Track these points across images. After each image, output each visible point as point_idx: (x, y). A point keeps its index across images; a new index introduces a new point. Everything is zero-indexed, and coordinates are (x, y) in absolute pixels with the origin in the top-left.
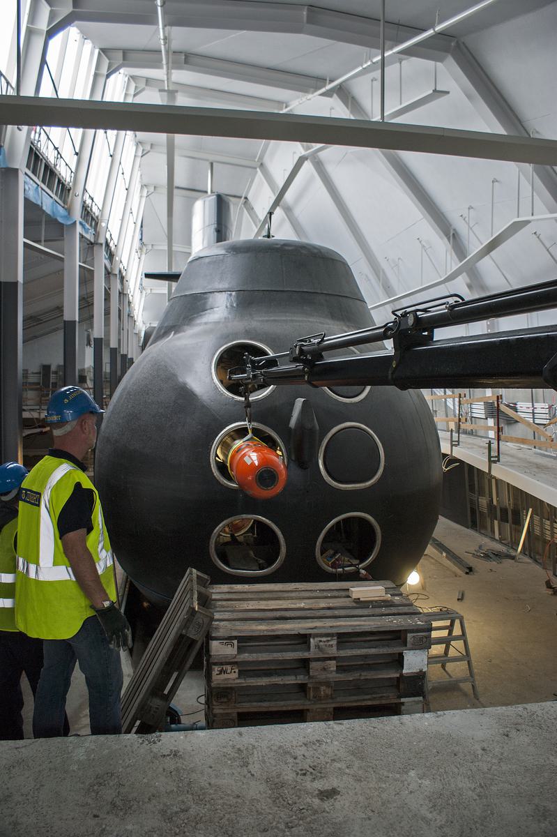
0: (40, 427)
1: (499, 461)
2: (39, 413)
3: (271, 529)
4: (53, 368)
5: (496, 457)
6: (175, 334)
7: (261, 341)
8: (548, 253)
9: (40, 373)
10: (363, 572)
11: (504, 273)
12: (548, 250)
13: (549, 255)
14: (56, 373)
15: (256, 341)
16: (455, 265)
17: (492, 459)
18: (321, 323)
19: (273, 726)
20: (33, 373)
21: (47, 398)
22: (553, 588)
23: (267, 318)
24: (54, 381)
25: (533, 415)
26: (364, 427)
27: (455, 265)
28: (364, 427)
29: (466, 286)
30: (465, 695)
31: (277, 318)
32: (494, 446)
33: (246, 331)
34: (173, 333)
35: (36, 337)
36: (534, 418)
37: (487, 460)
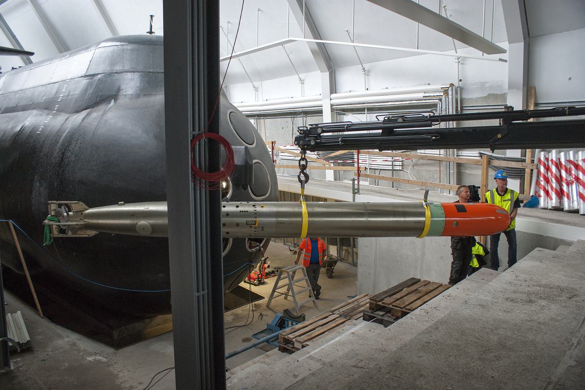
6: (115, 101)
10: (262, 249)
30: (310, 308)
34: (113, 100)
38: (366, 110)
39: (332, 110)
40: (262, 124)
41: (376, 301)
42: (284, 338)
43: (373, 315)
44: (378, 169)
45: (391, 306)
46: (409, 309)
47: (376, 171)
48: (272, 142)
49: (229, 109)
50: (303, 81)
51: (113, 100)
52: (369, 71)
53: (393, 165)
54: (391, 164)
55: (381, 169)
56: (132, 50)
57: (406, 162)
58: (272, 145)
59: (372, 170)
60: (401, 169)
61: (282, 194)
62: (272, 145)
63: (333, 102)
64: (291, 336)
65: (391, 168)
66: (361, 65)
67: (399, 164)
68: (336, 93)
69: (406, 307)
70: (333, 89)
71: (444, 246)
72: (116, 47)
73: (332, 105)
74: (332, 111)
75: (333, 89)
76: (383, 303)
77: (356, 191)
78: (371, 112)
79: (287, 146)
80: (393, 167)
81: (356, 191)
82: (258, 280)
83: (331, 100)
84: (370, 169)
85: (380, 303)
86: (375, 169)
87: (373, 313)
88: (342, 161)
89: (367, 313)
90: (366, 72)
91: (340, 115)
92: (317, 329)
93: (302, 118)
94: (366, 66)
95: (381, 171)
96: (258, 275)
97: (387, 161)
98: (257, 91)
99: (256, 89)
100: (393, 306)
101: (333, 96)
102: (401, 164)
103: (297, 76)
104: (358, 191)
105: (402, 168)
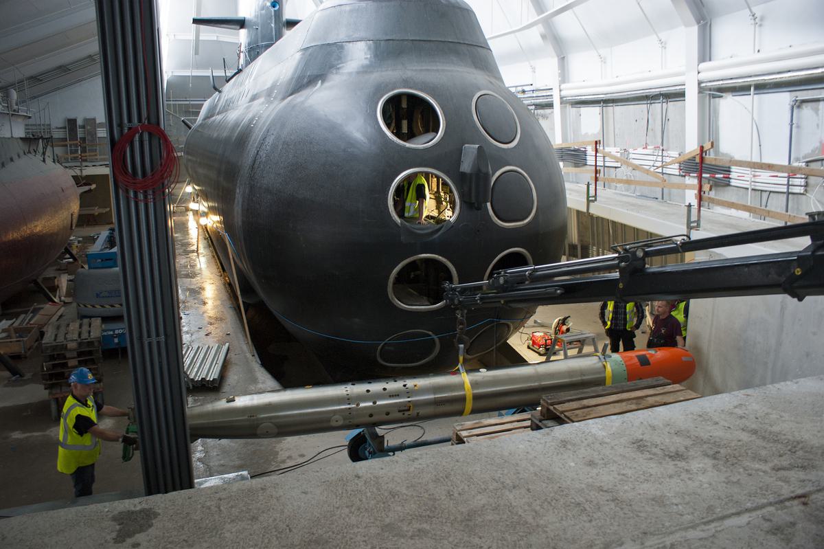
0: (85, 184)
1: (596, 200)
2: (81, 170)
3: (446, 267)
4: (80, 122)
5: (593, 197)
6: (322, 84)
7: (421, 90)
8: (638, 7)
9: (65, 128)
11: (585, 27)
12: (639, 4)
13: (639, 9)
14: (83, 127)
15: (416, 89)
16: (535, 17)
17: (590, 199)
18: (468, 72)
19: (321, 434)
20: (57, 128)
21: (75, 155)
22: (75, 340)
23: (420, 68)
24: (82, 136)
25: (604, 159)
26: (526, 175)
27: (535, 17)
28: (526, 175)
29: (540, 37)
31: (429, 68)
32: (592, 188)
33: (403, 80)
34: (320, 82)
35: (59, 89)
36: (604, 161)
37: (586, 200)
38: (752, 89)
39: (701, 90)
40: (611, 115)
41: (547, 403)
42: (457, 435)
43: (540, 424)
44: (766, 191)
45: (562, 416)
46: (568, 418)
47: (763, 193)
48: (596, 143)
49: (480, 89)
50: (665, 44)
51: (320, 82)
52: (762, 19)
53: (788, 185)
54: (786, 183)
55: (771, 192)
56: (351, 11)
57: (812, 180)
58: (596, 146)
59: (757, 192)
60: (802, 192)
61: (619, 227)
62: (596, 146)
63: (703, 76)
64: (464, 434)
65: (785, 190)
66: (748, 10)
67: (799, 184)
68: (710, 60)
69: (566, 414)
70: (705, 53)
71: (814, 334)
72: (333, 9)
73: (700, 83)
74: (700, 92)
75: (705, 53)
76: (554, 408)
77: (692, 225)
78: (761, 91)
79: (639, 149)
80: (788, 188)
81: (692, 225)
82: (545, 348)
83: (699, 73)
84: (753, 189)
85: (551, 408)
86: (762, 191)
87: (540, 422)
88: (722, 176)
89: (534, 419)
90: (758, 21)
91: (714, 97)
92: (513, 431)
93: (660, 104)
94: (758, 10)
95: (771, 194)
96: (546, 340)
97: (777, 176)
98: (605, 63)
99: (603, 60)
100: (565, 415)
101: (703, 65)
102: (803, 184)
103: (655, 36)
104: (698, 225)
105: (806, 191)
